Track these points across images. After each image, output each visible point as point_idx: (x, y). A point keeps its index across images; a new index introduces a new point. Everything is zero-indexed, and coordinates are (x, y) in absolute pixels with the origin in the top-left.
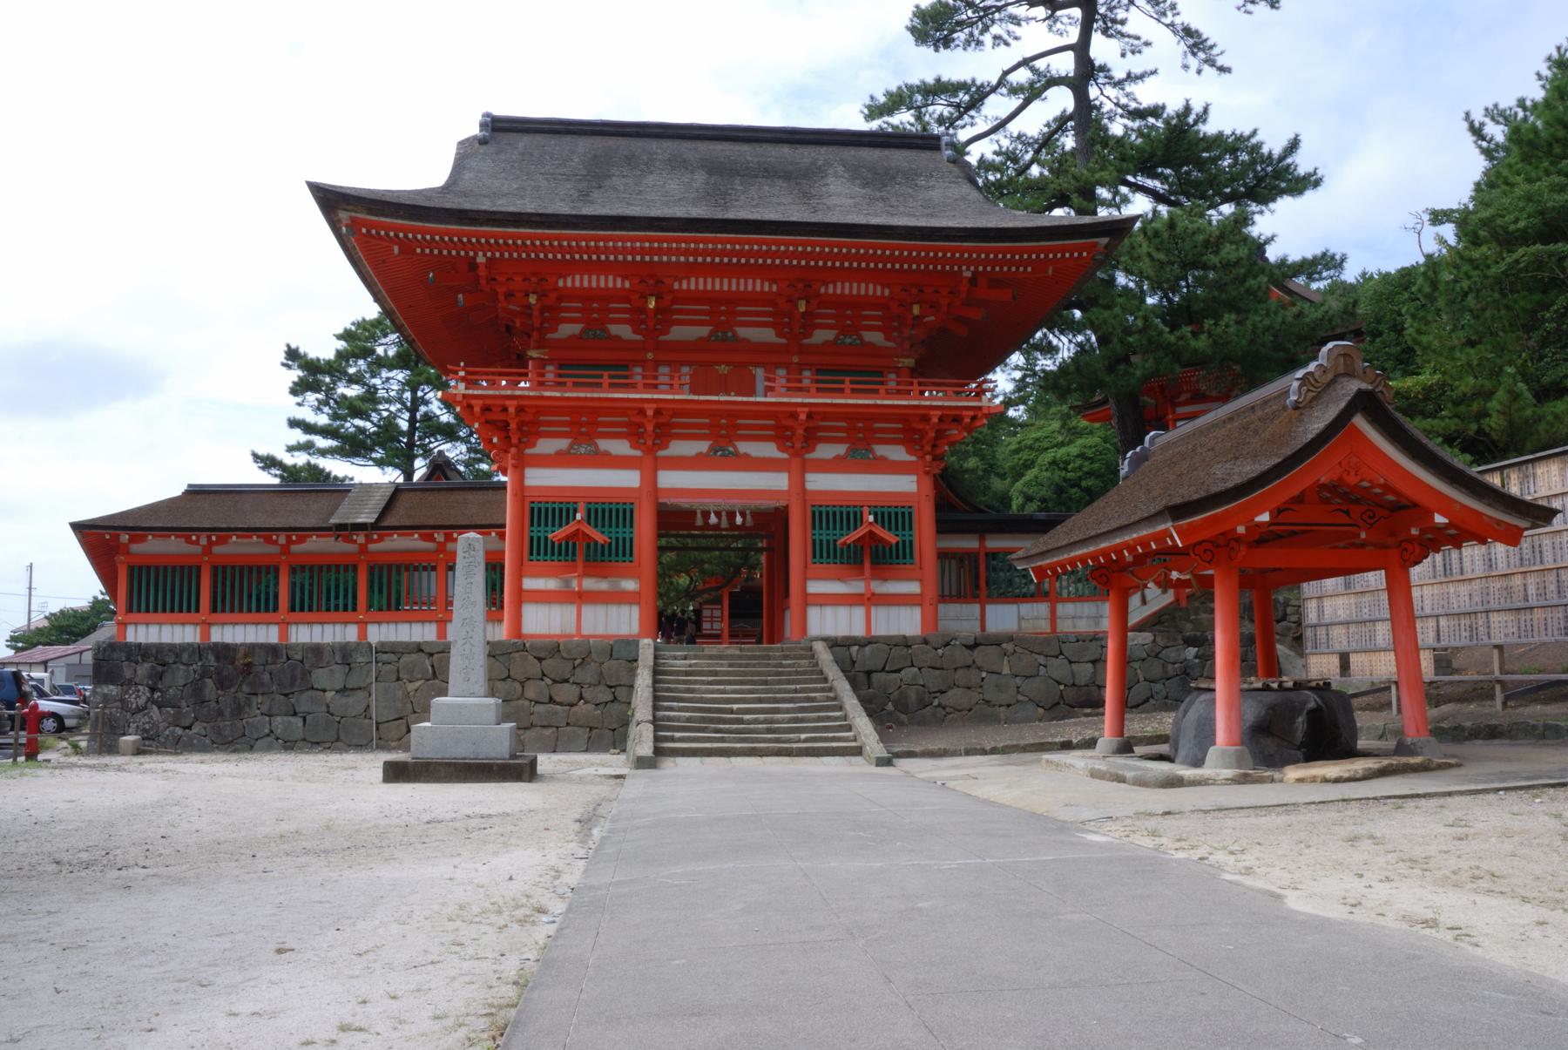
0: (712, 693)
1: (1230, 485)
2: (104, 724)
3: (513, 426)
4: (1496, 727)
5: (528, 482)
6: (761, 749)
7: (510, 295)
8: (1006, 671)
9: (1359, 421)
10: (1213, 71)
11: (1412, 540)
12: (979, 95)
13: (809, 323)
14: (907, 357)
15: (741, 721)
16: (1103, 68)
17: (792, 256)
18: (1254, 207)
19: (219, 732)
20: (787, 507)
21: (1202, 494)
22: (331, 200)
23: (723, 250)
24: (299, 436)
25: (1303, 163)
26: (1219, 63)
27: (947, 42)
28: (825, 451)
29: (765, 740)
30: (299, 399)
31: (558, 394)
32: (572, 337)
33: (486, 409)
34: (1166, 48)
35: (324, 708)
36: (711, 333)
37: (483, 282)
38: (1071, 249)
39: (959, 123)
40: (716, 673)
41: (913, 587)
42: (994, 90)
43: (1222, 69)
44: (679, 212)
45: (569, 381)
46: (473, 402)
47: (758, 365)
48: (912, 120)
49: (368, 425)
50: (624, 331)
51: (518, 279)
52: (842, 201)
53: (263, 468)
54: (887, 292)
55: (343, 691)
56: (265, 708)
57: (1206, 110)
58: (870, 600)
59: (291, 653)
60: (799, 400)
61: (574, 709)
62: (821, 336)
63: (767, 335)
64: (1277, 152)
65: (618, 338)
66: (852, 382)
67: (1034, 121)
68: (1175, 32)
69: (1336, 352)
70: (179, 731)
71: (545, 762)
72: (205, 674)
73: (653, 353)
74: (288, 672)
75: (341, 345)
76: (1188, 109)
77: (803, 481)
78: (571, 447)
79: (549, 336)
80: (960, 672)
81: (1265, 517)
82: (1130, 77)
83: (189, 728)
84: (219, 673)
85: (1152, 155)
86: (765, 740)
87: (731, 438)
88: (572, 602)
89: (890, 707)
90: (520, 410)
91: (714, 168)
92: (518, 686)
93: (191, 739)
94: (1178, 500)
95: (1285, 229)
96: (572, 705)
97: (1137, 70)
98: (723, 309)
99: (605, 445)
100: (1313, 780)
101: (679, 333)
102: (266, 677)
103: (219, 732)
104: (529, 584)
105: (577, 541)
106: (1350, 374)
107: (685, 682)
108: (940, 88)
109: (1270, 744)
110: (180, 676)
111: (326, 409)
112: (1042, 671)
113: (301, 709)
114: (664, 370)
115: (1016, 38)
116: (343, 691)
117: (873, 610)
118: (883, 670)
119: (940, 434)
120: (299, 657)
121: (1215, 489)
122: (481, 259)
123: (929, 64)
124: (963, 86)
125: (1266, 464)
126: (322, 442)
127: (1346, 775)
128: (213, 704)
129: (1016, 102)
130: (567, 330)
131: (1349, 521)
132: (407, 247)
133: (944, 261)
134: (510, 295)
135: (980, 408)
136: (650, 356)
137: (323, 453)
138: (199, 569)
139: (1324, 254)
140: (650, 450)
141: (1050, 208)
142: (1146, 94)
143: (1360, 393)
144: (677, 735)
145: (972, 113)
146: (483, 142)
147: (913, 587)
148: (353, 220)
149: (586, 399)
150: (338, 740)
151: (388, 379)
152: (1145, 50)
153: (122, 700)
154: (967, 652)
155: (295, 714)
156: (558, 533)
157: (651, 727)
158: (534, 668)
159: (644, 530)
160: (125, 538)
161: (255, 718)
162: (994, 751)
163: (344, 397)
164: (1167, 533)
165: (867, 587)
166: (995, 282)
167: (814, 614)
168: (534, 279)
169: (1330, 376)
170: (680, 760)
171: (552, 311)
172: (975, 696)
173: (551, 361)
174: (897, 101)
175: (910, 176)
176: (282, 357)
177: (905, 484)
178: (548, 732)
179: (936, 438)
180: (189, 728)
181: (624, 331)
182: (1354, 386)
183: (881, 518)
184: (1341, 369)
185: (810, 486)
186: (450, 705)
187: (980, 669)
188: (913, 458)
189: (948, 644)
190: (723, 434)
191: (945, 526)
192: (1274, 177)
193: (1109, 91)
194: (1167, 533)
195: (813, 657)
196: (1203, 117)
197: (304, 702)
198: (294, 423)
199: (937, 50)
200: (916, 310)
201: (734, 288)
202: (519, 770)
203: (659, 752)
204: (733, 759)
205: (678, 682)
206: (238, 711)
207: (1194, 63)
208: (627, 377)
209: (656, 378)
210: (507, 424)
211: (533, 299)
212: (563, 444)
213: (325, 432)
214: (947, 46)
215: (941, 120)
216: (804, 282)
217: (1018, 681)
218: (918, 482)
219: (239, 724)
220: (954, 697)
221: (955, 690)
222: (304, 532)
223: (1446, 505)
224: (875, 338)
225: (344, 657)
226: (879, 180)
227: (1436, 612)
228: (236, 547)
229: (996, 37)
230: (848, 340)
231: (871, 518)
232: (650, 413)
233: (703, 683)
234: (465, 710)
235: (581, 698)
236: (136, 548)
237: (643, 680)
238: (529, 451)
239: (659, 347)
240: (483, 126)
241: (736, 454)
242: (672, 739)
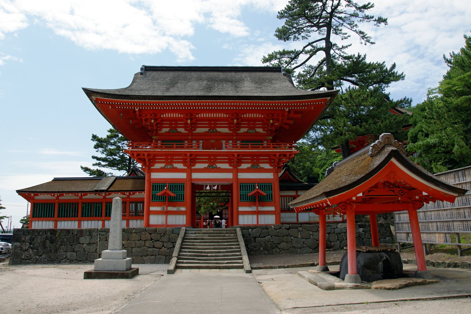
0: (199, 246)
1: (347, 184)
2: (14, 255)
3: (147, 160)
4: (456, 263)
5: (152, 177)
6: (210, 266)
7: (146, 120)
8: (300, 237)
9: (393, 160)
10: (369, 44)
11: (416, 200)
12: (297, 54)
13: (239, 126)
14: (270, 136)
15: (207, 256)
16: (335, 45)
17: (231, 106)
18: (384, 85)
19: (50, 257)
20: (232, 184)
21: (337, 187)
22: (89, 93)
23: (226, 105)
24: (95, 161)
25: (398, 70)
26: (371, 42)
27: (288, 39)
28: (244, 166)
29: (213, 263)
30: (97, 150)
31: (160, 150)
32: (166, 132)
33: (138, 155)
34: (355, 38)
35: (83, 250)
36: (209, 130)
37: (138, 116)
38: (318, 101)
39: (292, 63)
40: (203, 239)
41: (272, 209)
42: (301, 52)
43: (372, 43)
44: (195, 94)
45: (164, 146)
46: (134, 153)
47: (223, 140)
48: (278, 63)
49: (116, 157)
50: (182, 130)
51: (149, 115)
52: (248, 88)
53: (84, 171)
54: (263, 116)
55: (89, 244)
56: (65, 250)
57: (365, 56)
58: (258, 213)
59: (73, 232)
60: (235, 151)
61: (161, 250)
62: (243, 130)
63: (226, 130)
64: (388, 69)
65: (180, 132)
66: (251, 145)
67: (315, 61)
68: (357, 33)
69: (384, 136)
70: (38, 257)
71: (142, 268)
72: (47, 238)
73: (192, 137)
74: (73, 237)
75: (109, 134)
76: (359, 56)
77: (237, 176)
78: (165, 166)
79: (159, 132)
80: (285, 237)
81: (361, 195)
82: (343, 47)
83: (41, 256)
84: (51, 238)
85: (349, 71)
86: (213, 263)
87: (215, 163)
88: (164, 214)
89: (262, 249)
90: (149, 155)
91: (210, 80)
92: (143, 242)
93: (41, 259)
94: (328, 190)
95: (394, 91)
96: (160, 248)
97: (345, 45)
98: (213, 123)
99: (175, 165)
100: (381, 288)
101: (199, 130)
102: (65, 240)
103: (50, 257)
104: (152, 209)
105: (168, 195)
106: (390, 145)
107: (193, 242)
108: (283, 53)
109: (369, 272)
110: (39, 240)
111: (105, 153)
112: (312, 236)
113: (76, 250)
114: (194, 142)
115: (310, 36)
116: (89, 244)
117: (259, 216)
118: (259, 237)
119: (280, 160)
120: (76, 233)
121: (341, 186)
122: (137, 110)
123: (281, 46)
124: (292, 52)
125: (360, 176)
126: (103, 163)
127: (392, 287)
128: (49, 248)
129: (308, 56)
130: (165, 130)
131: (394, 194)
132: (113, 106)
133: (281, 106)
134: (146, 120)
135: (292, 152)
136: (190, 137)
137: (104, 166)
138: (55, 204)
139: (405, 99)
140: (189, 167)
141: (319, 88)
142: (349, 52)
143: (392, 151)
144: (185, 261)
145: (296, 60)
146: (141, 74)
147: (272, 209)
148: (97, 99)
149: (169, 151)
150: (87, 260)
151: (124, 143)
152: (349, 38)
153: (21, 247)
154: (286, 230)
155: (74, 251)
156: (159, 193)
157: (176, 259)
158: (149, 237)
159: (188, 192)
160: (32, 195)
161: (61, 252)
162: (288, 267)
163: (110, 149)
164: (326, 202)
165: (257, 209)
166: (296, 112)
167: (241, 217)
168: (153, 115)
169: (382, 145)
170: (184, 270)
171: (160, 123)
172: (290, 245)
173: (160, 140)
174: (271, 57)
175: (270, 81)
176: (91, 138)
177: (270, 176)
178: (152, 257)
179: (279, 161)
180: (41, 256)
181: (182, 130)
182: (390, 149)
183: (260, 187)
184: (387, 142)
185: (239, 177)
186: (108, 253)
187: (291, 236)
188: (272, 168)
189: (280, 228)
190: (212, 163)
191: (282, 188)
192: (387, 75)
193: (337, 51)
194: (326, 202)
195: (236, 233)
196: (364, 58)
197: (77, 248)
198: (94, 157)
199: (285, 41)
200: (271, 121)
201: (215, 116)
202: (130, 274)
203: (177, 267)
204: (201, 270)
205: (190, 242)
206: (56, 251)
207: (363, 41)
208: (183, 145)
209: (192, 145)
210: (145, 160)
211: (153, 121)
212: (162, 165)
213: (104, 160)
214: (288, 40)
215: (286, 62)
216: (236, 114)
217: (304, 240)
218: (274, 175)
219: (56, 255)
220: (283, 245)
221: (283, 243)
222: (86, 193)
223: (427, 189)
224: (260, 130)
225: (89, 234)
226: (259, 82)
227: (436, 220)
228: (66, 197)
229: (303, 37)
230: (251, 131)
231: (257, 187)
232: (188, 155)
233: (198, 242)
234: (113, 254)
235: (163, 246)
236: (36, 198)
237: (179, 241)
238: (152, 168)
239: (193, 135)
240: (142, 69)
241: (216, 168)
242: (183, 263)
